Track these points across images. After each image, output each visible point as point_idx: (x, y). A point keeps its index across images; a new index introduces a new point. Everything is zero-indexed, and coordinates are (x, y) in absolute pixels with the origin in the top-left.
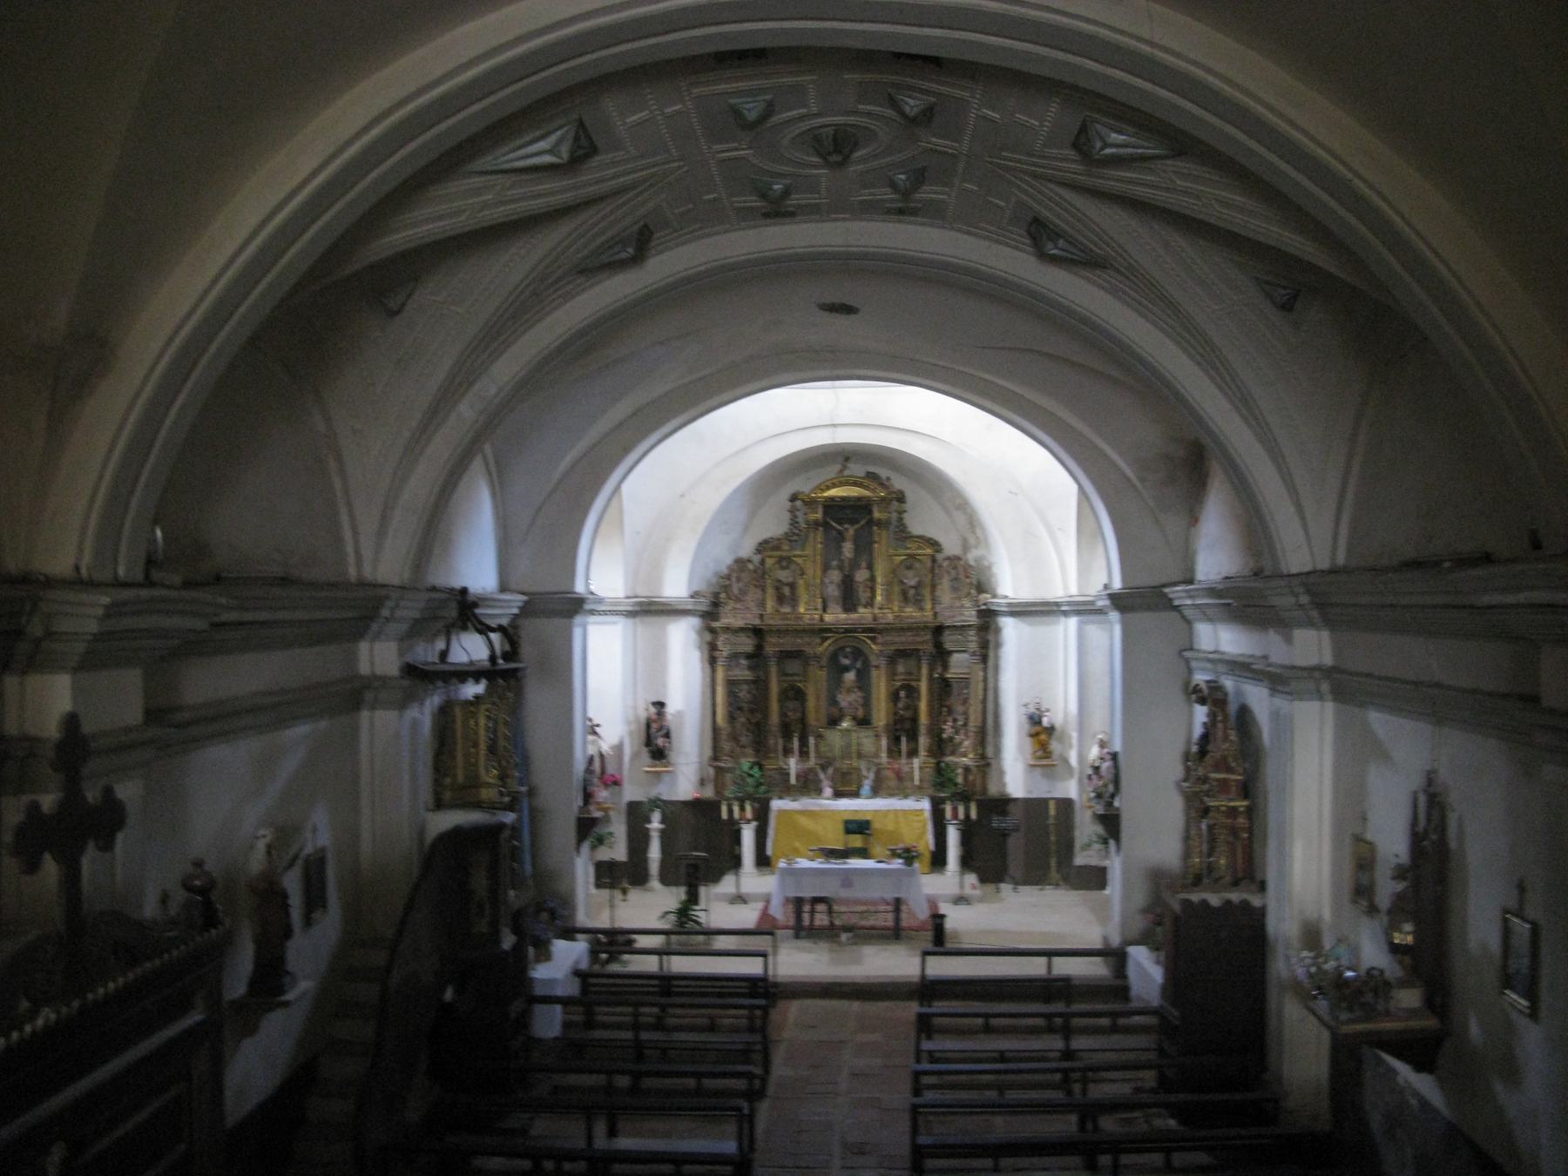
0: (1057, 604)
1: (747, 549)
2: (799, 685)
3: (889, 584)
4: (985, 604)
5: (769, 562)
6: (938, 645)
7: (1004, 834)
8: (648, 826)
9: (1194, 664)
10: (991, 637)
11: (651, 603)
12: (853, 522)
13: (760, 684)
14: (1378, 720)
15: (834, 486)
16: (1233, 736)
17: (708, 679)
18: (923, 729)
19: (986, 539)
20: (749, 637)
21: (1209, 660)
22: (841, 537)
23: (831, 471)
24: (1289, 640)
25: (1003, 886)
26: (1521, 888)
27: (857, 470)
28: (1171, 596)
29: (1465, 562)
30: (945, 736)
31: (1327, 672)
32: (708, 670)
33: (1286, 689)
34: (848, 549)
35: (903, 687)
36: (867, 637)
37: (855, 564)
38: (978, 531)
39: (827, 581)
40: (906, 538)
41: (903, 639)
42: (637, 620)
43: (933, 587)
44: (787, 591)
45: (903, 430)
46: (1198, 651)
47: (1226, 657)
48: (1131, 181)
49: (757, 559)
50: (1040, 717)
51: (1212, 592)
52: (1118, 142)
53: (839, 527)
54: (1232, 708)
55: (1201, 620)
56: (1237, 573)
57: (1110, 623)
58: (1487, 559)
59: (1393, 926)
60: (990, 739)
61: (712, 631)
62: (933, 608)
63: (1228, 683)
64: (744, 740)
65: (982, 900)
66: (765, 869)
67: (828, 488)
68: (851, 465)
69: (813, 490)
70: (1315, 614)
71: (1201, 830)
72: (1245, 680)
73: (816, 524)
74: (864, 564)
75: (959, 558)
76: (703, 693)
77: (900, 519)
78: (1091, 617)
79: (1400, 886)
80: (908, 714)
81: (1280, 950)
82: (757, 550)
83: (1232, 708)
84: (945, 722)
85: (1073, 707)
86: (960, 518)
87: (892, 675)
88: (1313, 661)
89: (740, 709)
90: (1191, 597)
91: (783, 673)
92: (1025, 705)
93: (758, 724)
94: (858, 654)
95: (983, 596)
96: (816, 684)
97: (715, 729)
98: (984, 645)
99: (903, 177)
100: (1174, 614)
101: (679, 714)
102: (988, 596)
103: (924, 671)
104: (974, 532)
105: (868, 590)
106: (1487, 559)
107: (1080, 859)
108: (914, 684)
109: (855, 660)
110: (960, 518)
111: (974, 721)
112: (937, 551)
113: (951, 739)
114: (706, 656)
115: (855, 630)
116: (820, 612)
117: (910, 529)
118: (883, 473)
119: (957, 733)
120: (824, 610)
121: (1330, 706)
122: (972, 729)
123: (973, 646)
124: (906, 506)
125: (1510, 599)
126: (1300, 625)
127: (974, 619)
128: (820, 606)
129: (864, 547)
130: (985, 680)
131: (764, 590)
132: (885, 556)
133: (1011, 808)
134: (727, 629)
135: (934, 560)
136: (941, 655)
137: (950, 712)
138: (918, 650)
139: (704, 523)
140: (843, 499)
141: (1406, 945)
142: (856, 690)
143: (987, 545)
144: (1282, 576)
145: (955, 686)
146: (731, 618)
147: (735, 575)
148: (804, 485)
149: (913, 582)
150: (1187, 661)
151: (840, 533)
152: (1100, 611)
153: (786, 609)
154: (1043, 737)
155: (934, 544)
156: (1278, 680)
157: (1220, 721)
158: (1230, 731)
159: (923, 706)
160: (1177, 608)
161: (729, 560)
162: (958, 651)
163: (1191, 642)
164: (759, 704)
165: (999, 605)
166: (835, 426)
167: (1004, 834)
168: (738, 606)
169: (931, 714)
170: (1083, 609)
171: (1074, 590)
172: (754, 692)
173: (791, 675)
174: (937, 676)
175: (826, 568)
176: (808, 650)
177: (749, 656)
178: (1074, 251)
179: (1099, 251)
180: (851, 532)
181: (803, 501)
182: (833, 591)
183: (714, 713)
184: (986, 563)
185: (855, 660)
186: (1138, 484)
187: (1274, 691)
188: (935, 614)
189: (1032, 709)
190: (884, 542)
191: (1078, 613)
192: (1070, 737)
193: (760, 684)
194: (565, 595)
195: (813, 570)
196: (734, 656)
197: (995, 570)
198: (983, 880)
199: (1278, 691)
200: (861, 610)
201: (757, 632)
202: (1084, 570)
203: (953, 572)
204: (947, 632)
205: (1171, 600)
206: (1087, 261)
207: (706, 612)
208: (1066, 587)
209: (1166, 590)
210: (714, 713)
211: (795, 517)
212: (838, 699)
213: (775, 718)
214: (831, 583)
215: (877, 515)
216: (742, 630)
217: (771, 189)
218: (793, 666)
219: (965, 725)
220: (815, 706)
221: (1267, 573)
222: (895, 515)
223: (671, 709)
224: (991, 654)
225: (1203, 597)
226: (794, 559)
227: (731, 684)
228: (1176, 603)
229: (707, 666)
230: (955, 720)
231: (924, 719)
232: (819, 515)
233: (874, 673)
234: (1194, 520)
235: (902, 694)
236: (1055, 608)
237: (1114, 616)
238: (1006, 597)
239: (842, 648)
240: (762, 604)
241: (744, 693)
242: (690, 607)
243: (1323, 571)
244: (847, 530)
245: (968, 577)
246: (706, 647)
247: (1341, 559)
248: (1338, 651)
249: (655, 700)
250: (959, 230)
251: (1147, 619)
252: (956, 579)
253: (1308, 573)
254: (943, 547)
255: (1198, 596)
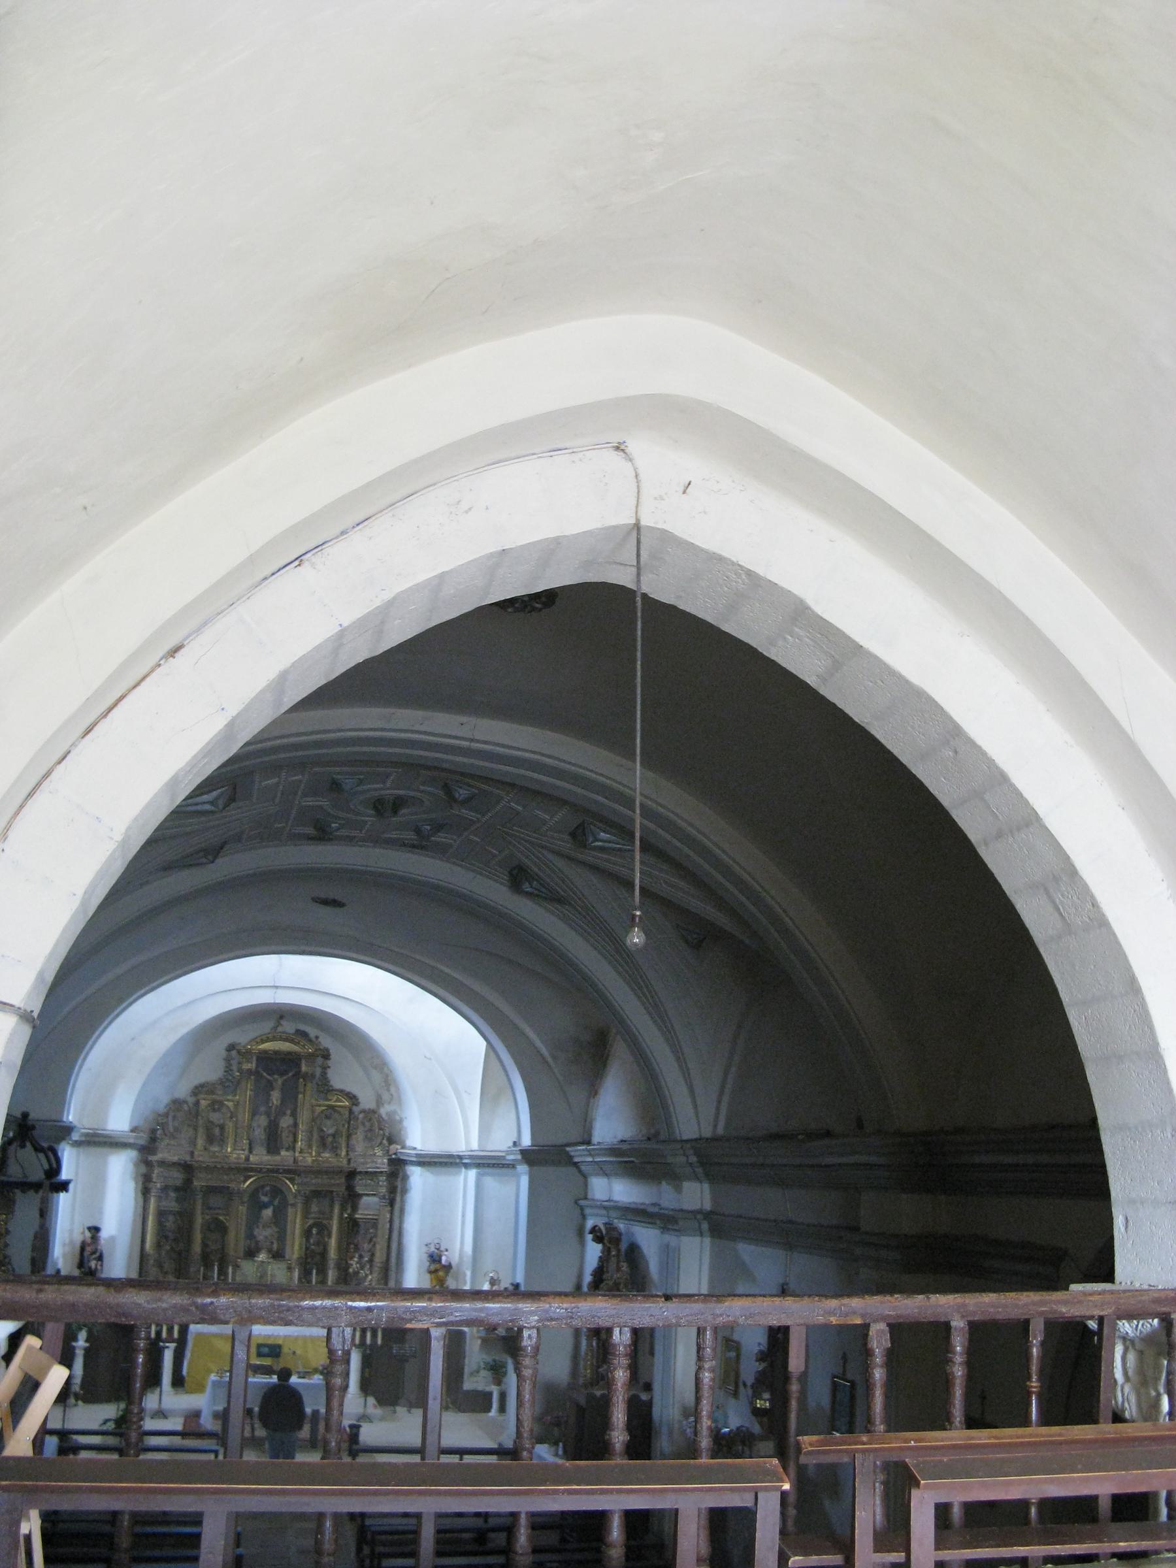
0: (460, 1157)
1: (183, 1091)
2: (221, 1218)
3: (310, 1132)
4: (395, 1154)
5: (203, 1103)
6: (350, 1188)
7: (403, 1360)
8: (74, 1344)
9: (588, 1211)
10: (399, 1184)
11: (95, 1135)
12: (282, 1075)
13: (186, 1216)
14: (746, 1251)
15: (268, 1040)
16: (625, 1267)
17: (140, 1210)
18: (331, 1264)
19: (399, 1097)
20: (178, 1171)
21: (605, 1208)
22: (270, 1086)
23: (266, 1027)
24: (678, 1189)
25: (398, 1409)
26: (845, 1358)
27: (289, 1027)
28: (572, 1154)
29: (811, 1136)
30: (351, 1270)
31: (707, 1215)
32: (141, 1201)
33: (676, 1227)
34: (275, 1097)
35: (314, 1225)
36: (286, 1178)
37: (281, 1113)
38: (393, 1089)
39: (254, 1124)
40: (328, 1091)
41: (320, 1181)
42: (81, 1150)
43: (349, 1136)
44: (217, 1131)
45: (339, 996)
46: (593, 1200)
47: (619, 1205)
48: (608, 861)
49: (191, 1100)
50: (440, 1257)
51: (613, 1151)
52: (605, 839)
53: (269, 1077)
54: (624, 1246)
55: (597, 1175)
56: (631, 1137)
57: (518, 1176)
58: (828, 1134)
59: (757, 1395)
60: (392, 1274)
61: (148, 1164)
62: (347, 1154)
63: (621, 1226)
64: (166, 1266)
65: (382, 1419)
66: (180, 1389)
67: (263, 1041)
68: (284, 1022)
69: (250, 1042)
70: (699, 1170)
71: (592, 1346)
72: (636, 1223)
73: (250, 1072)
74: (289, 1112)
75: (374, 1112)
76: (134, 1220)
77: (324, 1074)
78: (487, 1170)
79: (761, 1366)
80: (319, 1249)
81: (665, 1430)
82: (193, 1092)
83: (624, 1246)
84: (351, 1258)
85: (468, 1248)
86: (376, 1076)
87: (306, 1214)
88: (697, 1207)
89: (166, 1237)
90: (591, 1155)
91: (207, 1207)
92: (427, 1245)
93: (180, 1254)
94: (277, 1192)
95: (393, 1147)
96: (237, 1218)
97: (143, 1256)
98: (393, 1190)
99: (429, 828)
100: (573, 1170)
101: (112, 1239)
102: (399, 1147)
103: (336, 1211)
104: (388, 1090)
105: (291, 1136)
106: (828, 1134)
107: (467, 1385)
108: (325, 1222)
109: (273, 1197)
110: (376, 1076)
111: (379, 1257)
112: (353, 1104)
113: (356, 1273)
114: (140, 1186)
115: (277, 1171)
116: (246, 1152)
117: (332, 1083)
118: (312, 1032)
119: (362, 1268)
120: (251, 1151)
121: (707, 1241)
122: (379, 1265)
123: (383, 1190)
124: (330, 1063)
125: (844, 1160)
126: (689, 1179)
127: (386, 1166)
128: (247, 1147)
129: (290, 1097)
130: (391, 1221)
131: (195, 1129)
132: (309, 1102)
133: (408, 1336)
134: (162, 1163)
135: (351, 1112)
136: (352, 1198)
137: (357, 1248)
138: (332, 1192)
139: (152, 1063)
140: (276, 1052)
141: (766, 1409)
142: (272, 1225)
143: (400, 1102)
144: (676, 1141)
145: (362, 1225)
146: (166, 1153)
147: (171, 1114)
148: (236, 1037)
149: (331, 1131)
150: (582, 1209)
151: (269, 1081)
152: (512, 1166)
153: (216, 1149)
154: (441, 1273)
155: (353, 1098)
156: (666, 1220)
157: (614, 1256)
158: (622, 1264)
159: (333, 1242)
160: (576, 1164)
161: (165, 1100)
162: (368, 1195)
163: (586, 1195)
164: (184, 1233)
165: (408, 1155)
166: (277, 987)
167: (403, 1360)
168: (172, 1142)
169: (339, 1249)
170: (488, 1163)
171: (475, 1145)
172: (179, 1222)
173: (215, 1209)
174: (346, 1216)
175: (254, 1113)
176: (232, 1185)
177: (177, 1189)
178: (544, 890)
179: (563, 893)
180: (280, 1081)
181: (239, 1052)
182: (259, 1133)
183: (143, 1241)
184: (398, 1118)
185: (273, 1197)
186: (550, 1060)
187: (664, 1229)
188: (349, 1161)
189: (433, 1249)
190: (308, 1093)
191: (478, 1166)
192: (465, 1275)
193: (186, 1216)
194: (56, 1123)
195: (244, 1116)
196: (165, 1189)
197: (405, 1123)
198: (381, 1402)
199: (668, 1229)
200: (283, 1153)
201: (188, 1168)
202: (485, 1129)
203: (368, 1124)
204: (358, 1177)
205: (571, 1157)
206: (552, 897)
207: (142, 1145)
208: (468, 1142)
209: (568, 1149)
210: (143, 1241)
211: (231, 1065)
212: (255, 1233)
213: (197, 1248)
214: (259, 1126)
215: (304, 1068)
216: (174, 1164)
217: (330, 826)
218: (216, 1201)
219: (371, 1261)
220: (235, 1239)
221: (662, 1137)
222: (318, 1071)
223: (104, 1234)
224: (398, 1199)
225: (604, 1155)
226: (226, 1103)
227: (161, 1214)
228: (576, 1160)
229: (140, 1195)
230: (361, 1257)
231: (332, 1254)
232: (252, 1065)
233: (290, 1210)
234: (593, 1092)
235: (314, 1231)
236: (458, 1161)
237: (523, 1169)
238: (415, 1149)
239: (263, 1187)
240: (193, 1143)
241: (170, 1223)
242: (132, 1141)
243: (707, 1139)
244: (276, 1080)
245: (381, 1129)
246: (141, 1180)
247: (720, 1131)
248: (714, 1199)
249: (90, 1225)
250: (454, 863)
251: (550, 1172)
252: (371, 1130)
253: (696, 1140)
254: (360, 1100)
255: (598, 1155)
